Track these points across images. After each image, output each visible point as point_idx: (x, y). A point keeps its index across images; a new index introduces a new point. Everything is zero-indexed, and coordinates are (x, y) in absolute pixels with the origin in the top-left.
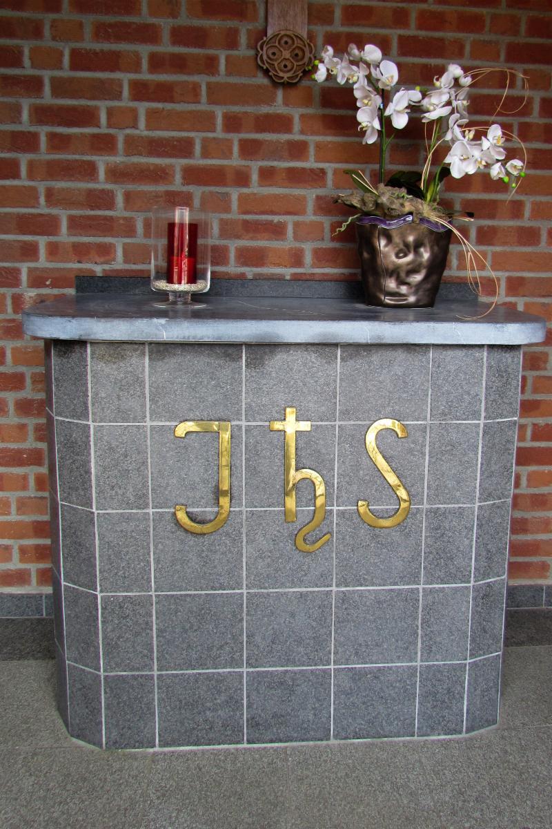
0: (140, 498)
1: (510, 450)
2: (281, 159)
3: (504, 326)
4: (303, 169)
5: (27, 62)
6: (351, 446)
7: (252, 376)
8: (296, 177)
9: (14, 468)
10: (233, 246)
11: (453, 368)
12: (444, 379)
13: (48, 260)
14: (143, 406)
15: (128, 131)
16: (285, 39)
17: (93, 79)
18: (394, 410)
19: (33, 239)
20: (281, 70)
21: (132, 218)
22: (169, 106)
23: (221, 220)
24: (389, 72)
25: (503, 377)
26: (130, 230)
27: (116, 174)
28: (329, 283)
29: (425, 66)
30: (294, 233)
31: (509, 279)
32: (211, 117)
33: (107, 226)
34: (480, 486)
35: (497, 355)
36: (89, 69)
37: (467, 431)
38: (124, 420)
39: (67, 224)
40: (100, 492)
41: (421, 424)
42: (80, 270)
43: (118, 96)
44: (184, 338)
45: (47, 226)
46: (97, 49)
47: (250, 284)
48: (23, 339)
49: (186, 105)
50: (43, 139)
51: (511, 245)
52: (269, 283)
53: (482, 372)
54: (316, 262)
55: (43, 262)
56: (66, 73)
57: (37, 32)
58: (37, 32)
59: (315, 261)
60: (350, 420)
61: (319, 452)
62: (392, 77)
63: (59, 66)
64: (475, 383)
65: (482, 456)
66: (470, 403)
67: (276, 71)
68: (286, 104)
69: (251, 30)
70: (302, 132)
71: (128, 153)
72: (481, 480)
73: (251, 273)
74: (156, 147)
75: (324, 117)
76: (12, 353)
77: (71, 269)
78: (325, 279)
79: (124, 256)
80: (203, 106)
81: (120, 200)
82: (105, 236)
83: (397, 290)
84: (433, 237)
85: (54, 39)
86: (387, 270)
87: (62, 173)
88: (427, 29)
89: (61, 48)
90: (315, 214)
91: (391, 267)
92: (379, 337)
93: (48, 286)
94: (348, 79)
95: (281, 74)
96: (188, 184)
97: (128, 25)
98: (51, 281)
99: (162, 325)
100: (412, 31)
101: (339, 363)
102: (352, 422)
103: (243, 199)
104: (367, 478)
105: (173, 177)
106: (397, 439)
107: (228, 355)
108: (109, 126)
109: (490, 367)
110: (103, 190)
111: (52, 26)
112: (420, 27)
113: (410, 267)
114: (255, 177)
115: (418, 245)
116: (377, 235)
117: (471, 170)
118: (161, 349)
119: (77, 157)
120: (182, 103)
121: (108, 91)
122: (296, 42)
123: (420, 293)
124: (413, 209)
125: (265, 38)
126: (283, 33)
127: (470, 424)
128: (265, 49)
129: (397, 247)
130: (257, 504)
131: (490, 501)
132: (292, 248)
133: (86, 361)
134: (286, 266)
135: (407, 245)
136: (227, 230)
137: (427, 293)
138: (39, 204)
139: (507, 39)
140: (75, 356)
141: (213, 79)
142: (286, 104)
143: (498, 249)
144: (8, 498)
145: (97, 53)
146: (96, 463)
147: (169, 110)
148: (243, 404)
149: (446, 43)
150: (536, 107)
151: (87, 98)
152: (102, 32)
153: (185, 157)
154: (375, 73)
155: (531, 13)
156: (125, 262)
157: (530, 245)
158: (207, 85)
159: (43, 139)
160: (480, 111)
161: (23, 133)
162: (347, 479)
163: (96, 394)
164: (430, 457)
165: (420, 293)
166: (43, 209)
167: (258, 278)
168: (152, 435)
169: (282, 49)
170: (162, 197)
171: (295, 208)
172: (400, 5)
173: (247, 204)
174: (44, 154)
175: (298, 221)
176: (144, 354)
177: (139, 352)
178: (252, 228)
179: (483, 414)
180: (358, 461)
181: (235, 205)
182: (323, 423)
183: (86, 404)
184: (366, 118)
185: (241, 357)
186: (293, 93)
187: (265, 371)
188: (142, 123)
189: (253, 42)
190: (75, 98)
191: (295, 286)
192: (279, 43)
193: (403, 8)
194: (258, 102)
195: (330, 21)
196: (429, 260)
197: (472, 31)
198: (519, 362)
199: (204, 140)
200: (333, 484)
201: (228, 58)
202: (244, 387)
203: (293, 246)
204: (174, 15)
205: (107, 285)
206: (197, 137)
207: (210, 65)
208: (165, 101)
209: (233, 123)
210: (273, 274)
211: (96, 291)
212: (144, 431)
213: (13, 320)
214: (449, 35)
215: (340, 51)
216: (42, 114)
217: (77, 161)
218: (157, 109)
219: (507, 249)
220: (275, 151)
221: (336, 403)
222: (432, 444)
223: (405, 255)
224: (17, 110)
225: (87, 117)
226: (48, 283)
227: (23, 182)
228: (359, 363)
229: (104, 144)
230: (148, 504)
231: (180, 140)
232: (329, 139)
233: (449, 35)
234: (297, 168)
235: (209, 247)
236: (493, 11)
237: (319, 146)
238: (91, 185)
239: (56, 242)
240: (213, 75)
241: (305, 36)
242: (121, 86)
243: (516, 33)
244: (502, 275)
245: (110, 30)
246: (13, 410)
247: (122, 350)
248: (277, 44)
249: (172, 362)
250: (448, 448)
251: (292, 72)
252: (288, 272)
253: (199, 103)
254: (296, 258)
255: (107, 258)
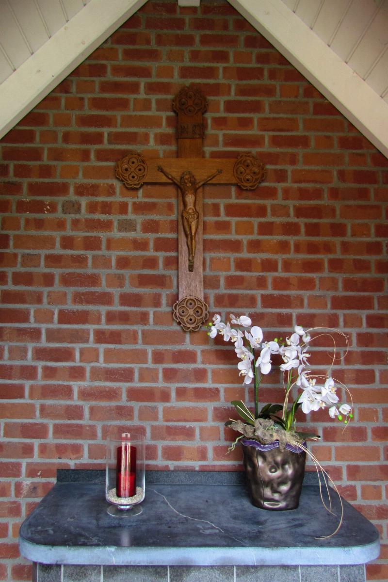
2: (190, 381)
3: (350, 549)
4: (205, 389)
5: (32, 319)
8: (201, 394)
10: (160, 445)
13: (40, 457)
15: (93, 364)
16: (190, 301)
17: (73, 330)
20: (188, 323)
22: (118, 346)
23: (152, 426)
24: (257, 334)
26: (93, 436)
27: (85, 394)
28: (225, 474)
30: (200, 435)
31: (349, 467)
32: (144, 353)
33: (78, 432)
36: (69, 323)
39: (53, 430)
42: (60, 464)
43: (87, 341)
44: (127, 562)
45: (38, 431)
46: (75, 310)
48: (21, 517)
50: (40, 371)
51: (347, 441)
52: (185, 474)
54: (216, 456)
55: (36, 458)
56: (55, 325)
58: (39, 300)
62: (259, 339)
63: (51, 321)
68: (192, 343)
70: (203, 363)
74: (110, 375)
75: (217, 351)
76: (13, 528)
77: (54, 464)
79: (119, 98)
80: (140, 346)
82: (77, 439)
83: (272, 497)
84: (294, 457)
85: (49, 303)
86: (264, 482)
88: (279, 289)
89: (53, 310)
90: (214, 420)
91: (267, 479)
92: (262, 560)
94: (231, 339)
95: (188, 326)
97: (93, 293)
98: (41, 473)
99: (112, 552)
103: (166, 411)
105: (121, 395)
108: (81, 361)
111: (48, 296)
112: (275, 288)
113: (280, 479)
114: (173, 395)
115: (284, 463)
116: (256, 455)
117: (316, 408)
119: (60, 383)
120: (126, 345)
121: (80, 337)
122: (197, 303)
125: (177, 302)
126: (188, 298)
128: (177, 308)
129: (270, 464)
132: (199, 447)
134: (195, 460)
135: (276, 463)
136: (157, 434)
137: (293, 499)
138: (36, 416)
139: (331, 293)
140: (53, 572)
141: (146, 328)
142: (192, 343)
149: (292, 298)
151: (68, 342)
152: (78, 298)
153: (129, 381)
154: (247, 335)
155: (345, 276)
156: (90, 457)
159: (40, 371)
160: (317, 359)
161: (27, 367)
166: (38, 419)
167: (177, 470)
169: (188, 309)
170: (113, 410)
171: (200, 417)
173: (169, 414)
174: (40, 381)
176: (100, 572)
178: (172, 432)
181: (161, 415)
184: (243, 367)
185: (167, 574)
186: (196, 336)
188: (101, 358)
189: (170, 302)
191: (202, 476)
194: (174, 342)
195: (217, 286)
196: (292, 473)
197: (307, 290)
198: (364, 573)
199: (141, 369)
201: (155, 313)
203: (200, 445)
204: (121, 286)
205: (77, 476)
206: (136, 367)
208: (116, 343)
209: (158, 357)
211: (70, 481)
213: (14, 502)
214: (292, 293)
215: (227, 320)
216: (40, 354)
218: (111, 349)
219: (345, 444)
220: (186, 376)
223: (276, 471)
224: (25, 351)
225: (67, 355)
226: (39, 474)
229: (77, 373)
231: (125, 370)
232: (221, 366)
233: (292, 293)
235: (144, 447)
237: (214, 372)
238: (69, 402)
239: (45, 443)
241: (202, 299)
242: (89, 334)
244: (343, 464)
246: (10, 574)
247: (84, 569)
248: (185, 305)
251: (195, 324)
252: (197, 464)
253: (137, 343)
255: (77, 455)
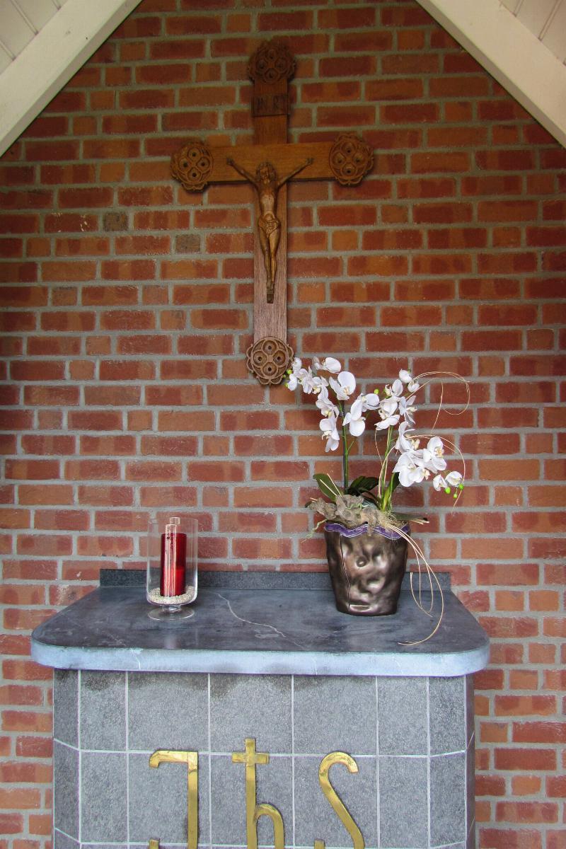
0: (120, 830)
1: (460, 785)
2: (269, 453)
4: (289, 463)
5: (67, 374)
6: (307, 780)
7: (217, 705)
8: (284, 470)
9: (45, 759)
11: (398, 698)
12: (390, 710)
14: (123, 734)
15: (145, 433)
18: (345, 743)
19: (68, 534)
20: (266, 374)
21: (147, 513)
22: (176, 408)
23: (221, 513)
25: (446, 707)
27: (135, 473)
29: (390, 360)
30: (283, 524)
31: (480, 567)
33: (125, 521)
34: (431, 828)
35: (439, 685)
36: (114, 379)
37: (415, 766)
38: (108, 747)
40: (86, 822)
41: (370, 758)
42: (104, 562)
43: (137, 402)
45: (78, 521)
47: (245, 576)
49: (191, 407)
50: (78, 442)
53: (426, 703)
55: (75, 555)
56: (96, 382)
57: (76, 349)
59: (301, 552)
60: (304, 752)
61: (277, 785)
64: (420, 715)
65: (431, 793)
66: (416, 736)
67: (262, 375)
69: (242, 336)
70: (287, 428)
71: (144, 453)
72: (432, 821)
73: (247, 565)
74: (167, 446)
77: (97, 562)
78: (309, 572)
80: (205, 407)
81: (137, 496)
84: (389, 545)
85: (88, 353)
87: (92, 473)
88: (390, 325)
89: (93, 362)
92: (325, 668)
93: (78, 578)
96: (192, 480)
99: (137, 656)
100: (378, 328)
101: (293, 692)
102: (307, 755)
103: (238, 493)
104: (323, 815)
106: (348, 774)
107: (196, 684)
108: (130, 428)
109: (433, 697)
110: (124, 488)
114: (248, 472)
115: (376, 553)
118: (139, 678)
119: (104, 457)
121: (127, 397)
122: (278, 347)
123: (381, 601)
124: (367, 520)
126: (266, 339)
127: (417, 759)
128: (252, 354)
130: (222, 841)
131: (443, 844)
133: (77, 688)
135: (365, 553)
137: (387, 601)
138: (73, 501)
139: (462, 329)
140: (70, 680)
141: (213, 382)
142: (272, 402)
143: (467, 536)
144: (38, 790)
145: (121, 364)
146: (83, 791)
147: (177, 412)
148: (209, 733)
150: (493, 393)
152: (125, 345)
154: (333, 384)
155: (482, 303)
157: (496, 531)
158: (207, 388)
159: (78, 442)
161: (62, 437)
162: (304, 815)
163: (84, 721)
164: (382, 794)
165: (381, 601)
166: (76, 506)
167: (252, 570)
168: (130, 763)
170: (170, 493)
171: (281, 500)
172: (366, 304)
175: (286, 513)
176: (124, 681)
177: (120, 680)
178: (246, 521)
179: (429, 748)
180: (313, 797)
182: (281, 755)
183: (76, 729)
185: (207, 686)
187: (228, 700)
190: (103, 405)
192: (264, 348)
193: (369, 307)
194: (250, 401)
197: (429, 324)
199: (206, 438)
200: (292, 820)
202: (209, 716)
204: (181, 326)
205: (124, 578)
206: (200, 435)
207: (210, 369)
208: (174, 404)
210: (265, 566)
212: (123, 760)
213: (49, 611)
214: (410, 329)
216: (79, 420)
217: (103, 461)
218: (167, 411)
219: (476, 536)
220: (264, 447)
221: (291, 734)
222: (382, 780)
223: (365, 564)
224: (58, 416)
226: (78, 575)
227: (61, 482)
228: (311, 692)
229: (125, 445)
230: (125, 837)
231: (185, 439)
233: (410, 329)
234: (283, 462)
236: (447, 303)
240: (212, 378)
242: (139, 392)
243: (470, 322)
244: (472, 563)
245: (131, 343)
248: (262, 350)
249: (148, 689)
250: (398, 785)
252: (277, 563)
253: (201, 404)
254: (285, 551)
